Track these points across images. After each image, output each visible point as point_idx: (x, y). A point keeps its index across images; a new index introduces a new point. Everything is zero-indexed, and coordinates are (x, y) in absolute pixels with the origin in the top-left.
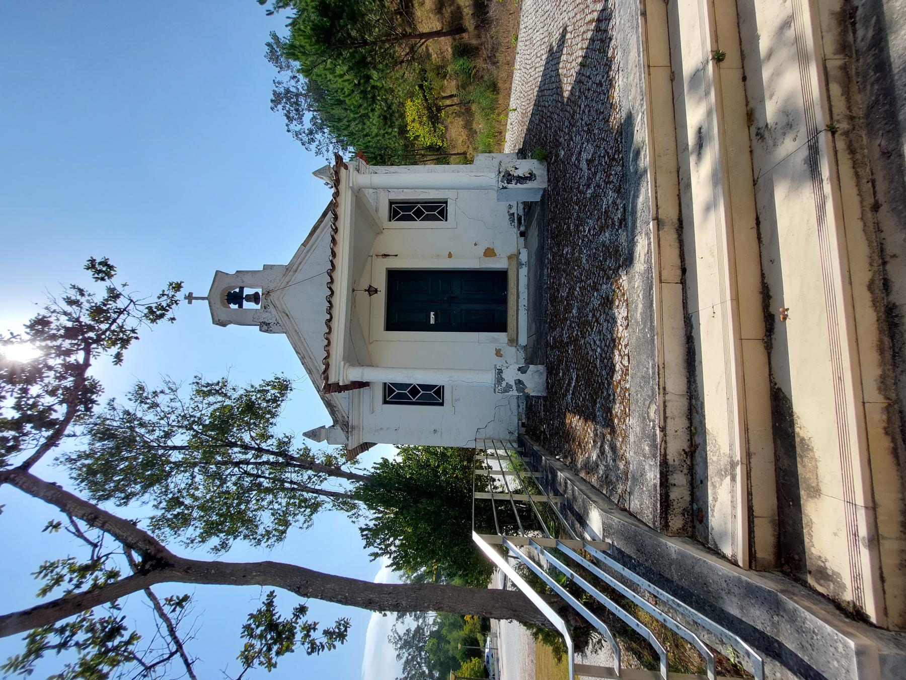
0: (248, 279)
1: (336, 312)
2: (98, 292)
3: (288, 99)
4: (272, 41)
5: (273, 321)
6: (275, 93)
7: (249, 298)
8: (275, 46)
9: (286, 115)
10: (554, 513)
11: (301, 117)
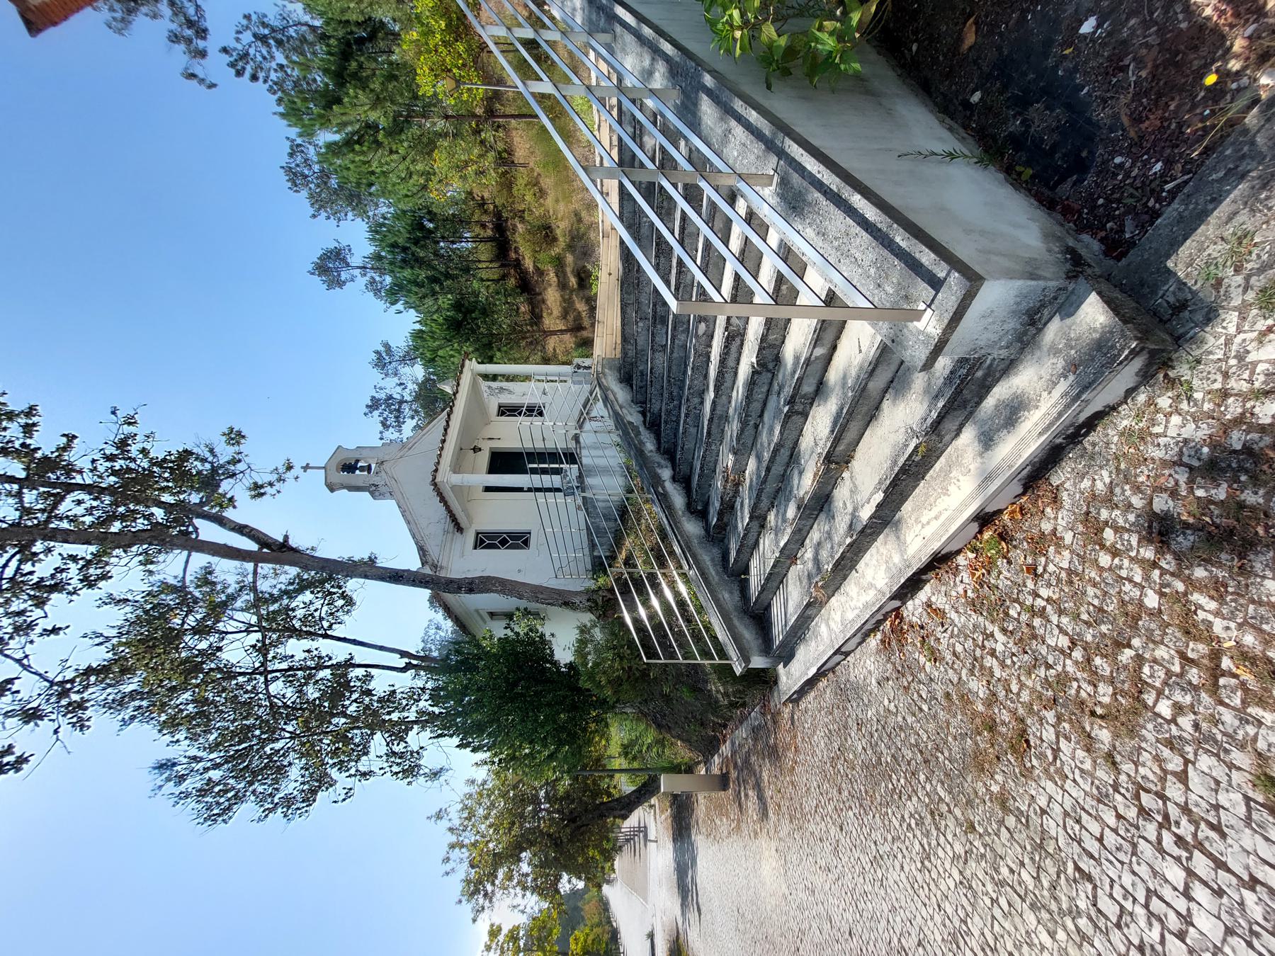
0: (365, 453)
1: (448, 438)
2: (225, 452)
3: (389, 406)
4: (383, 349)
5: (383, 483)
6: (373, 398)
7: (362, 469)
8: (384, 355)
9: (382, 422)
10: (585, 279)
11: (399, 424)
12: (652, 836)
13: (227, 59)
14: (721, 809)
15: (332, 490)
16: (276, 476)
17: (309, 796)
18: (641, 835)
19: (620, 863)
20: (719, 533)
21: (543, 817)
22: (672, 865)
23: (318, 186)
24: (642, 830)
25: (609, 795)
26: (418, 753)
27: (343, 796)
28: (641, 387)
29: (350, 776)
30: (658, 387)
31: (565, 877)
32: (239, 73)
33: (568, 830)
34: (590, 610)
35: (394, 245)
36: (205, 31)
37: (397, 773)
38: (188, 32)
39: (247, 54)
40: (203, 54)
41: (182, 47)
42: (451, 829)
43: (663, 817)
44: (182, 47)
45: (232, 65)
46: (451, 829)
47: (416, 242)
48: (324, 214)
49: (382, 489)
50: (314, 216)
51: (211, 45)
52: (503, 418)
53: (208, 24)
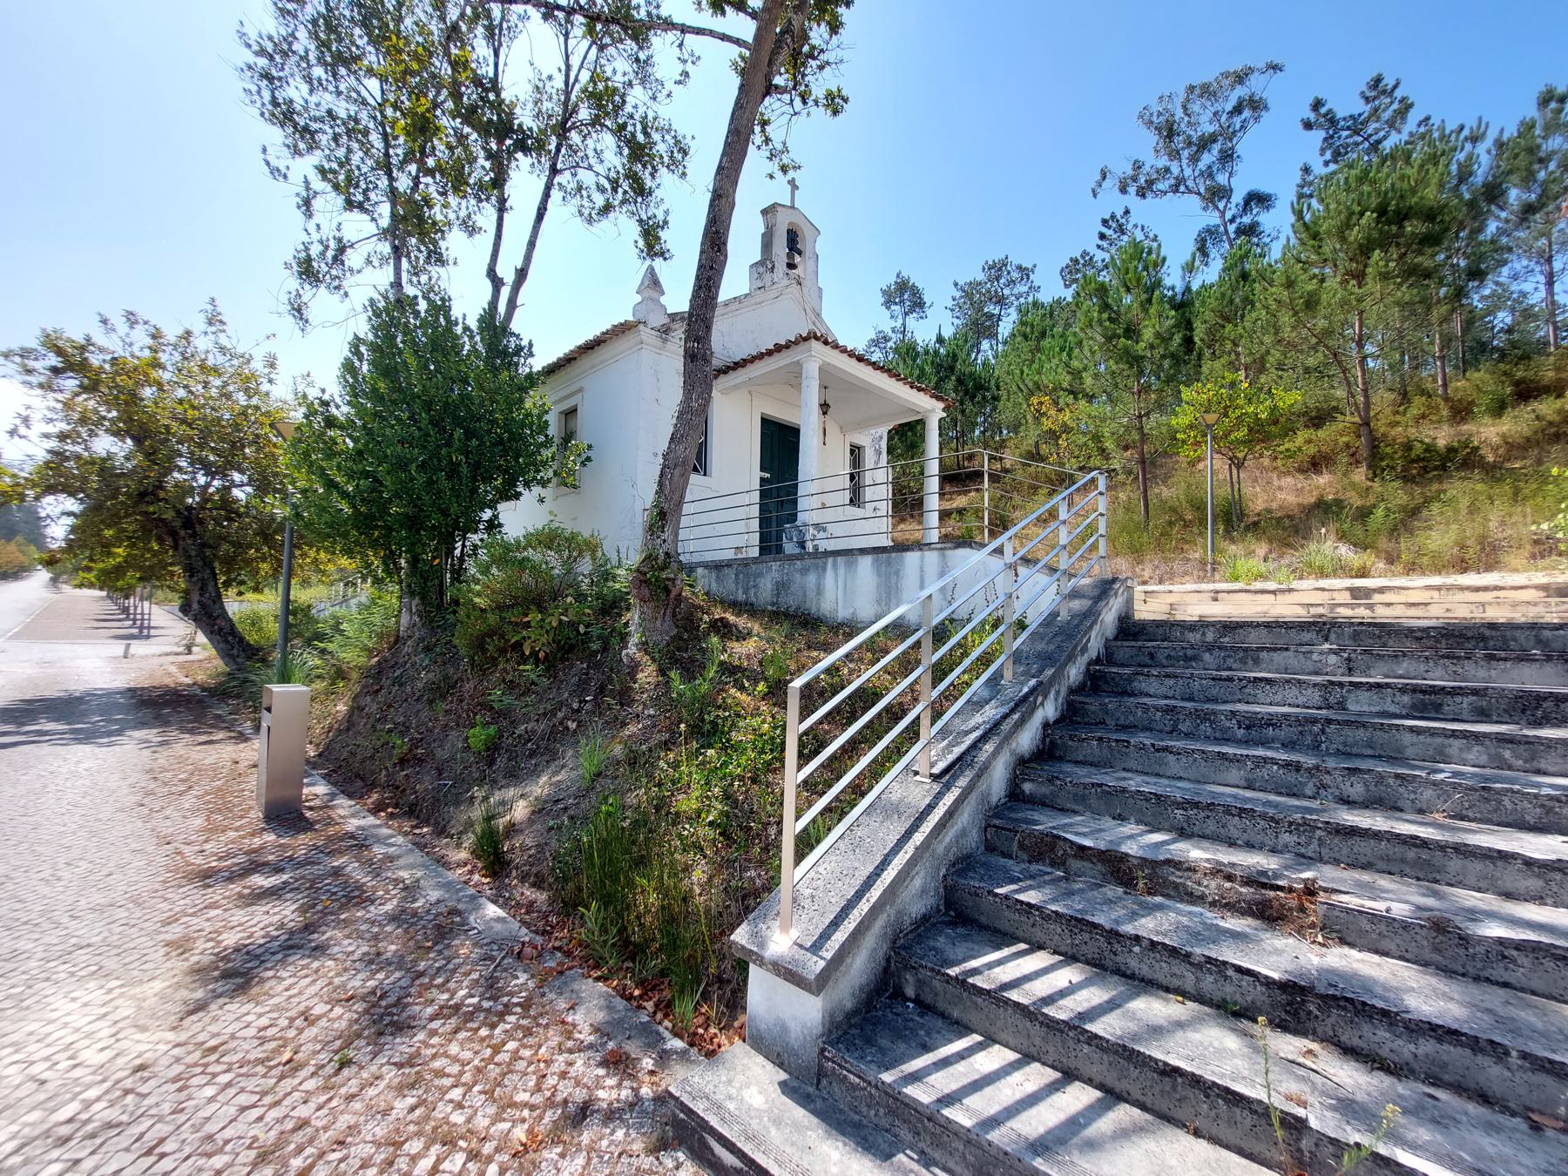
0: (810, 263)
2: (820, 84)
12: (138, 648)
13: (1119, 214)
14: (220, 807)
15: (765, 212)
16: (779, 147)
17: (284, 115)
18: (135, 631)
19: (91, 599)
20: (1022, 846)
21: (194, 479)
22: (77, 687)
23: (989, 291)
24: (143, 631)
25: (227, 584)
26: (338, 288)
27: (274, 163)
28: (1152, 656)
29: (307, 182)
30: (1214, 692)
31: (72, 505)
32: (1105, 222)
33: (169, 515)
34: (650, 558)
35: (955, 357)
36: (1143, 196)
37: (307, 249)
38: (1142, 180)
39: (1123, 233)
40: (1123, 190)
41: (1130, 172)
42: (188, 333)
43: (173, 669)
44: (1130, 172)
45: (1113, 217)
46: (188, 333)
47: (960, 381)
48: (958, 294)
49: (768, 277)
50: (956, 284)
51: (1131, 200)
52: (848, 449)
53: (1150, 198)
